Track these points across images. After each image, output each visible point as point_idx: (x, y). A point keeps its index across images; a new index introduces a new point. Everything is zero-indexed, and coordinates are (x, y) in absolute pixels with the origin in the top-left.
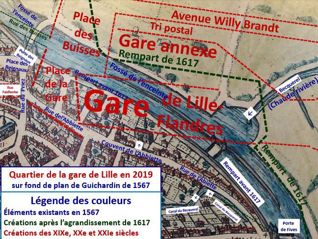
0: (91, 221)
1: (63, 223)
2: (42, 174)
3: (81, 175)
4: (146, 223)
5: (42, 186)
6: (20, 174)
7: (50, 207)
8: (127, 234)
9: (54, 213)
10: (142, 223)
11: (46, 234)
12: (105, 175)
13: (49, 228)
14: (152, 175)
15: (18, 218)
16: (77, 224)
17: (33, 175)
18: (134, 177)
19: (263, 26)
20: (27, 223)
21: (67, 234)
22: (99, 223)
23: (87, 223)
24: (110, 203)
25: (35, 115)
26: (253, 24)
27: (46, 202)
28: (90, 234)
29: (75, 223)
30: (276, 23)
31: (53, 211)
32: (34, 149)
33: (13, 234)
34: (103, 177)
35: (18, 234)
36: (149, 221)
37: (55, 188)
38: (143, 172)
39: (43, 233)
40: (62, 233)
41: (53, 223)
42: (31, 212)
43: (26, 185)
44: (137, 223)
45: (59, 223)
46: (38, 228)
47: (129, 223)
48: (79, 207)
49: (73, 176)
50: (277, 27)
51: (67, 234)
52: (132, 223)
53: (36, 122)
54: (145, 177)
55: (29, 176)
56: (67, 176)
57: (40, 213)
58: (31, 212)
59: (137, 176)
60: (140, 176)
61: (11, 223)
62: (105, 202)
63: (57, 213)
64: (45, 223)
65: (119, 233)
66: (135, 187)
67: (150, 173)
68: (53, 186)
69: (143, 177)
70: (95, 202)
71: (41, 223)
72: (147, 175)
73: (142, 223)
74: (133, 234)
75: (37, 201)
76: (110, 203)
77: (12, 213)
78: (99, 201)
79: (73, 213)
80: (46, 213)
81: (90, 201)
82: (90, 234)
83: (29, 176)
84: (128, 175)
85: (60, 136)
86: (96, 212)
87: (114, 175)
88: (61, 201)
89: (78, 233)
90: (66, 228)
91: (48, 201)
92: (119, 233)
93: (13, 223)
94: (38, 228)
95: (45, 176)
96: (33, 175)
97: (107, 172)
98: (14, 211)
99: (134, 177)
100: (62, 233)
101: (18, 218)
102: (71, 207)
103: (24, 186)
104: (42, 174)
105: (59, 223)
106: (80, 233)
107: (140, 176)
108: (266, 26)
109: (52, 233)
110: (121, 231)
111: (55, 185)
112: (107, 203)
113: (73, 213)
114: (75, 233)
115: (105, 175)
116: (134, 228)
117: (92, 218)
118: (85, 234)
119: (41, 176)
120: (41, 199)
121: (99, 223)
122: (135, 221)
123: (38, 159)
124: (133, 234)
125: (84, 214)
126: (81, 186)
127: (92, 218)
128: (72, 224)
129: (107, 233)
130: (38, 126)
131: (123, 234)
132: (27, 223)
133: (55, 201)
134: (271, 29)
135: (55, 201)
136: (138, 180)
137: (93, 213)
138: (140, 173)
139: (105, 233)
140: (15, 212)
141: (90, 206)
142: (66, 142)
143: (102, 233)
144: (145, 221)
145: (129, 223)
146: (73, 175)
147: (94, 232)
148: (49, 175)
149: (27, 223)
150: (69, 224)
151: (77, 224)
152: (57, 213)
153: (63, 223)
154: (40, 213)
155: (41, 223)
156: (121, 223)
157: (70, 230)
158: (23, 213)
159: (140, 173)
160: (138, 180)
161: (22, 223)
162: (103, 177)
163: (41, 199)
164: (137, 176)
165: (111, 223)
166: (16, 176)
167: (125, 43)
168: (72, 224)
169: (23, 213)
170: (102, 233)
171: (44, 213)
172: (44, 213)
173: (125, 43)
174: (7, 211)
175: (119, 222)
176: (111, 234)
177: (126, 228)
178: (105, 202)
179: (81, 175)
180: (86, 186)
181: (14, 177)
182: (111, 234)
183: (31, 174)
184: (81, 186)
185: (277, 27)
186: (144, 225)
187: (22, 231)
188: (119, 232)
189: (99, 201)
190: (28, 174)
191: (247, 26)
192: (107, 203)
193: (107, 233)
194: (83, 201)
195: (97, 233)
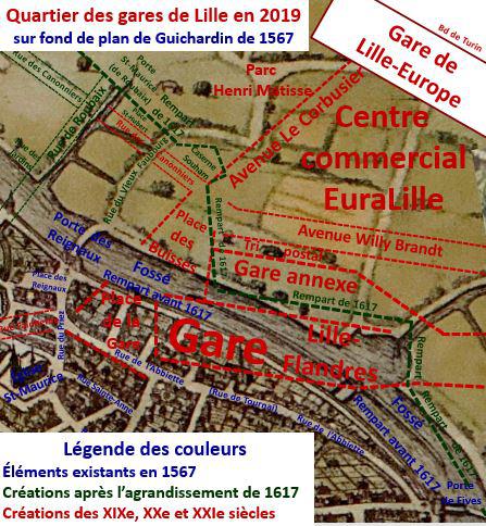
0: (179, 490)
1: (123, 493)
2: (75, 14)
3: (143, 17)
4: (291, 492)
5: (74, 39)
6: (29, 13)
7: (97, 462)
8: (253, 515)
9: (105, 473)
10: (283, 493)
11: (87, 515)
12: (201, 17)
13: (91, 504)
14: (299, 16)
15: (32, 483)
16: (152, 494)
17: (55, 17)
18: (262, 20)
19: (421, 247)
20: (49, 494)
21: (130, 515)
22: (196, 494)
23: (171, 493)
24: (377, 61)
25: (77, 350)
26: (407, 245)
27: (91, 452)
28: (178, 515)
29: (146, 494)
30: (439, 244)
31: (102, 470)
32: (76, 395)
33: (22, 515)
34: (197, 20)
35: (31, 515)
36: (297, 488)
37: (101, 43)
38: (280, 10)
39: (80, 514)
40: (122, 513)
41: (102, 494)
42: (57, 472)
43: (42, 37)
44: (272, 494)
45: (115, 493)
46: (73, 504)
47: (256, 494)
48: (151, 462)
49: (127, 18)
50: (440, 249)
51: (130, 515)
52: (264, 493)
53: (78, 360)
54: (286, 20)
55: (48, 17)
56: (116, 18)
57: (76, 473)
58: (57, 472)
59: (268, 17)
60: (275, 17)
61: (17, 494)
62: (199, 451)
63: (110, 474)
64: (444, 95)
65: (235, 514)
66: (263, 42)
67: (296, 13)
68: (96, 41)
69: (280, 20)
70: (180, 450)
71: (78, 494)
72: (290, 17)
73: (283, 493)
74: (264, 515)
75: (74, 450)
76: (377, 61)
77: (19, 473)
78: (188, 450)
79: (143, 473)
80: (88, 473)
81: (172, 450)
82: (178, 515)
83: (48, 17)
84: (249, 16)
85: (114, 377)
86: (189, 471)
87: (221, 16)
88: (119, 450)
89: (153, 513)
90: (129, 504)
91: (95, 450)
92: (235, 514)
93: (22, 494)
94: (73, 504)
95: (80, 17)
96: (55, 17)
97: (373, 44)
98: (23, 469)
99: (262, 20)
100: (122, 513)
101: (32, 483)
102: (137, 462)
103: (37, 40)
104: (75, 14)
105: (115, 493)
106: (157, 513)
107: (275, 17)
108: (425, 247)
109: (101, 513)
110: (241, 510)
111: (100, 37)
112: (202, 453)
113: (143, 473)
114: (148, 513)
115: (201, 17)
116: (264, 503)
117: (181, 483)
118: (166, 515)
119: (71, 18)
120: (82, 445)
121: (196, 494)
122: (268, 489)
123: (83, 407)
124: (264, 515)
125: (166, 475)
126: (153, 40)
127: (181, 483)
128: (141, 495)
129: (211, 513)
130: (81, 364)
131: (243, 515)
132: (49, 494)
133: (108, 450)
134: (432, 251)
135: (108, 450)
136: (269, 27)
137: (183, 473)
138: (275, 13)
139: (207, 513)
140: (26, 471)
141: (173, 460)
142: (123, 385)
143: (202, 513)
144: (289, 489)
145: (256, 494)
146: (128, 16)
147: (186, 512)
148: (89, 17)
149: (49, 514)
150: (135, 495)
151: (152, 494)
152: (110, 474)
153: (123, 493)
154: (76, 473)
155: (78, 494)
156: (240, 494)
157: (137, 507)
158: (42, 473)
159: (275, 13)
160: (269, 27)
161: (40, 494)
162: (197, 20)
163: (82, 445)
164: (268, 17)
165: (218, 494)
166: (20, 19)
167: (396, 36)
168: (141, 495)
169: (42, 473)
170: (202, 513)
171: (85, 473)
172: (85, 473)
173: (396, 36)
174: (10, 470)
175: (236, 491)
176: (220, 515)
177: (250, 504)
178: (199, 451)
179: (143, 17)
180: (163, 38)
181: (16, 20)
182: (220, 515)
183: (52, 13)
184: (153, 40)
185: (440, 249)
186: (286, 496)
187: (40, 510)
188: (236, 511)
189: (188, 450)
190: (45, 14)
191: (399, 247)
192: (202, 453)
193: (211, 513)
194: (159, 449)
195: (191, 513)
